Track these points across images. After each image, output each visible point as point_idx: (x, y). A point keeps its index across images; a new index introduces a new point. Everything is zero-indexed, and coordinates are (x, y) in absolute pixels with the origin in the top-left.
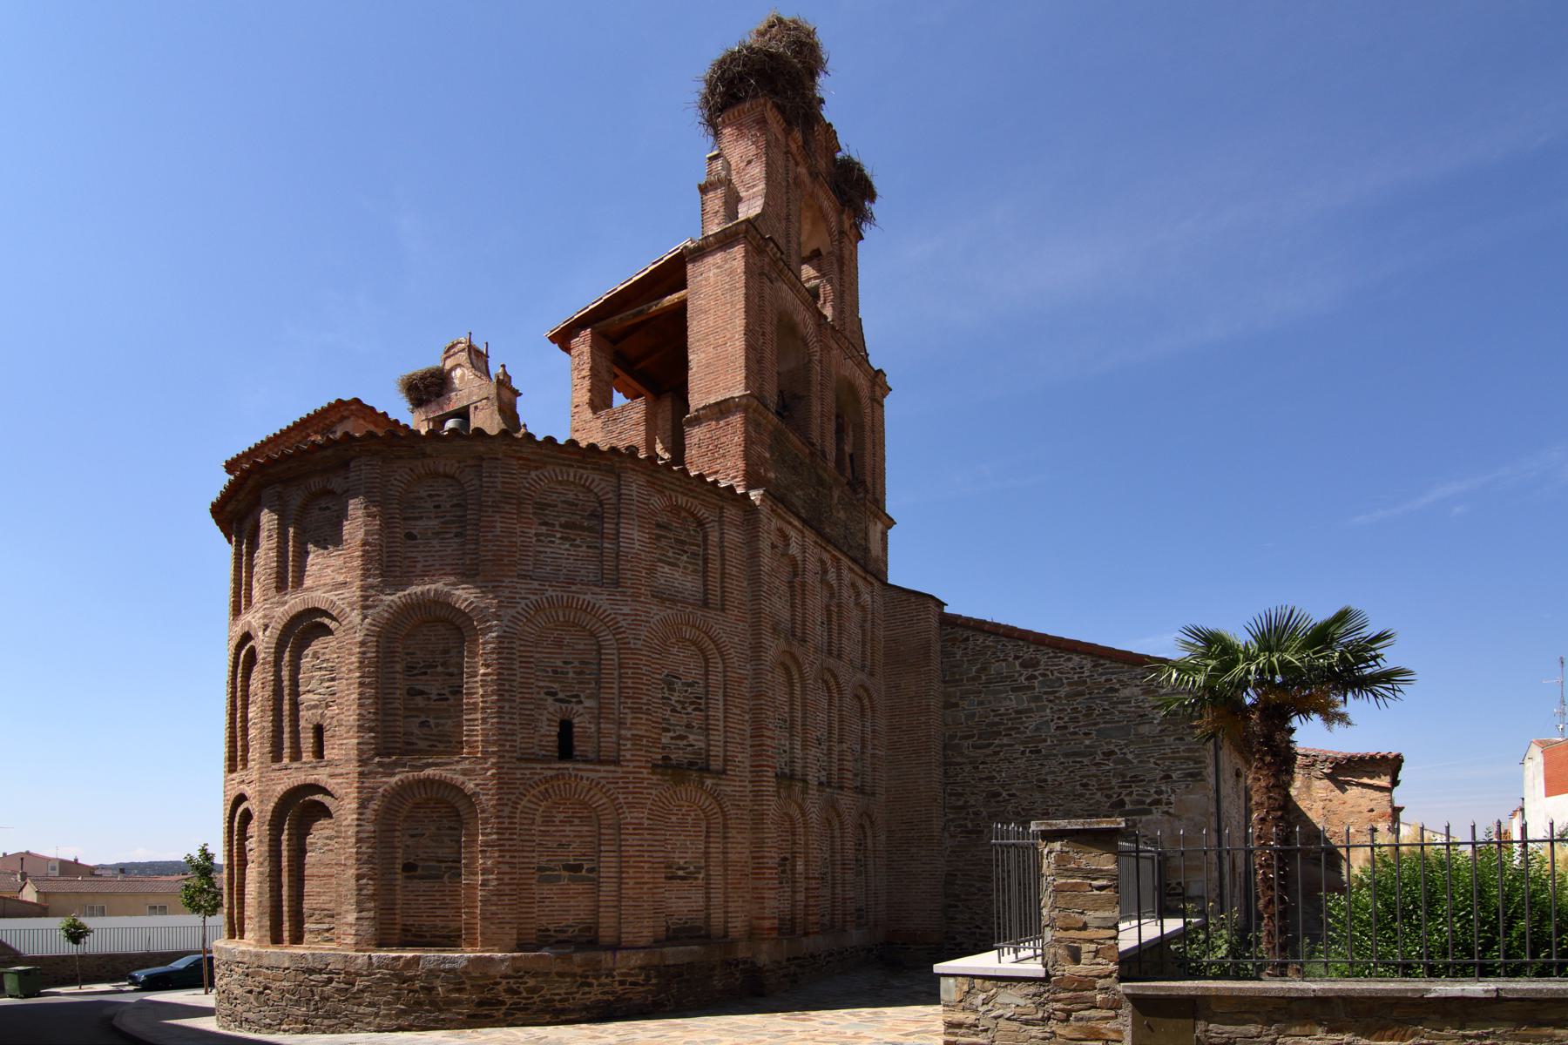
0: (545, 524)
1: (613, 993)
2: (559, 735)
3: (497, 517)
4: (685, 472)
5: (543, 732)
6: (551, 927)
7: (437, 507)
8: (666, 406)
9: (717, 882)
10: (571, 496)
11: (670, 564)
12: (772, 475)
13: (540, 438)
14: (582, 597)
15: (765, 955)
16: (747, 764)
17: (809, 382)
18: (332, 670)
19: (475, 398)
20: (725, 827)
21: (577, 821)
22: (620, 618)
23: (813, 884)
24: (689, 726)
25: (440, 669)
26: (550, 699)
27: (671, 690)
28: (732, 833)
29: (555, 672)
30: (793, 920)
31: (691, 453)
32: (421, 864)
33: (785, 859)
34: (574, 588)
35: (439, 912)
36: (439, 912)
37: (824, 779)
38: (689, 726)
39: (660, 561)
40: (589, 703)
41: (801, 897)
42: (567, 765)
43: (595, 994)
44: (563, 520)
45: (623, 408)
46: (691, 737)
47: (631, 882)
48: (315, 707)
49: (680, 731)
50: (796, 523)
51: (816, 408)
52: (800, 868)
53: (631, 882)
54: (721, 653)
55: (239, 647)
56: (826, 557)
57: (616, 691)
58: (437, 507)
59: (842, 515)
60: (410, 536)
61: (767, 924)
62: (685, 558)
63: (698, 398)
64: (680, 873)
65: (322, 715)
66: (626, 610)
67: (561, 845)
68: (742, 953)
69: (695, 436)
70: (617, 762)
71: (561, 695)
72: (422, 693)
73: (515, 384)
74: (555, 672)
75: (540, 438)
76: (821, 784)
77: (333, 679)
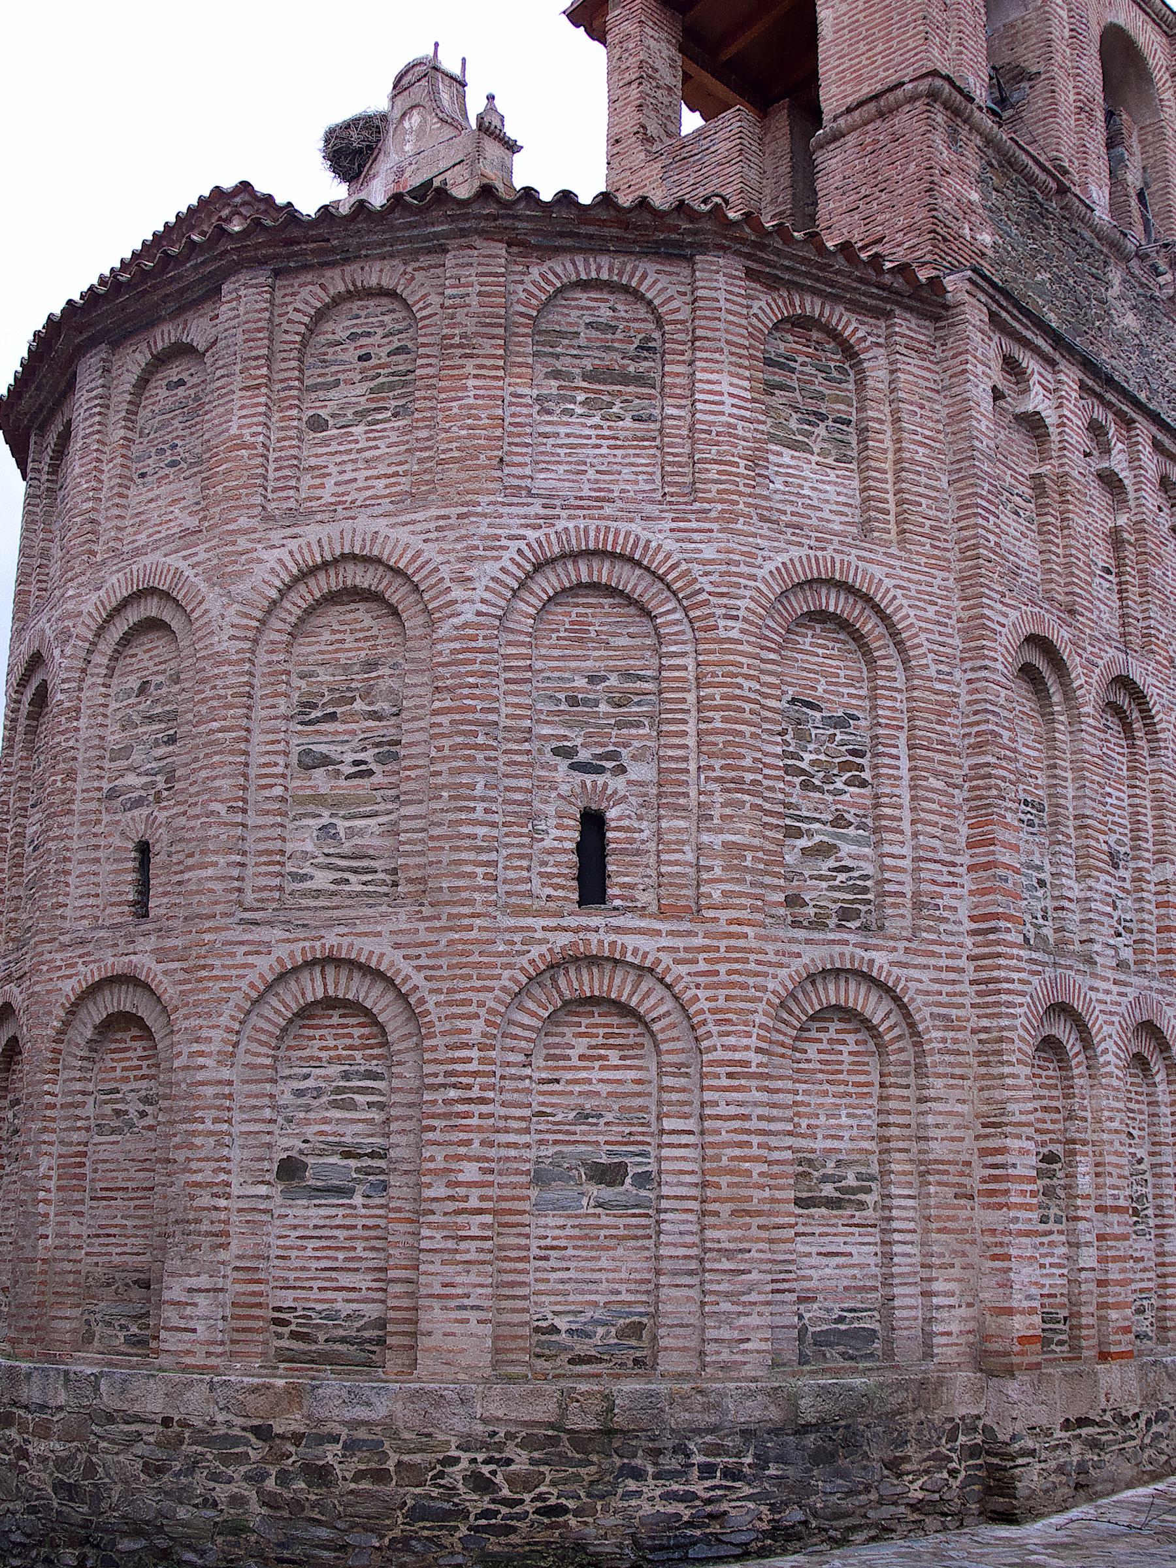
0: (556, 374)
1: (688, 1498)
2: (580, 848)
3: (470, 367)
4: (813, 238)
5: (548, 843)
6: (562, 1323)
7: (365, 358)
8: (781, 121)
9: (904, 1213)
10: (605, 313)
11: (794, 446)
12: (986, 238)
13: (546, 196)
14: (624, 526)
15: (1024, 1408)
16: (963, 914)
17: (1049, 43)
18: (172, 716)
19: (443, 165)
20: (920, 1070)
21: (614, 1057)
22: (697, 569)
23: (1116, 1223)
24: (839, 821)
25: (359, 705)
26: (563, 764)
27: (803, 737)
28: (938, 1086)
29: (573, 701)
30: (1073, 1303)
31: (829, 208)
32: (310, 1161)
33: (1050, 1158)
34: (608, 510)
35: (345, 1280)
36: (345, 1280)
37: (1127, 954)
38: (839, 821)
39: (773, 439)
40: (641, 771)
41: (1088, 1257)
42: (595, 921)
43: (62, 664)
44: (588, 364)
45: (699, 133)
46: (846, 848)
47: (725, 1209)
48: (139, 802)
49: (821, 834)
50: (1040, 342)
51: (1067, 98)
52: (1084, 1183)
53: (725, 1209)
54: (899, 645)
55: (23, 683)
56: (1100, 413)
57: (691, 741)
58: (365, 358)
59: (1130, 321)
60: (317, 424)
61: (1019, 1325)
62: (821, 430)
63: (833, 95)
64: (828, 1190)
65: (150, 820)
66: (709, 553)
67: (583, 1117)
68: (963, 1399)
69: (836, 165)
70: (695, 912)
71: (584, 755)
72: (325, 761)
73: (511, 131)
74: (573, 701)
75: (546, 196)
76: (1121, 965)
77: (172, 740)
